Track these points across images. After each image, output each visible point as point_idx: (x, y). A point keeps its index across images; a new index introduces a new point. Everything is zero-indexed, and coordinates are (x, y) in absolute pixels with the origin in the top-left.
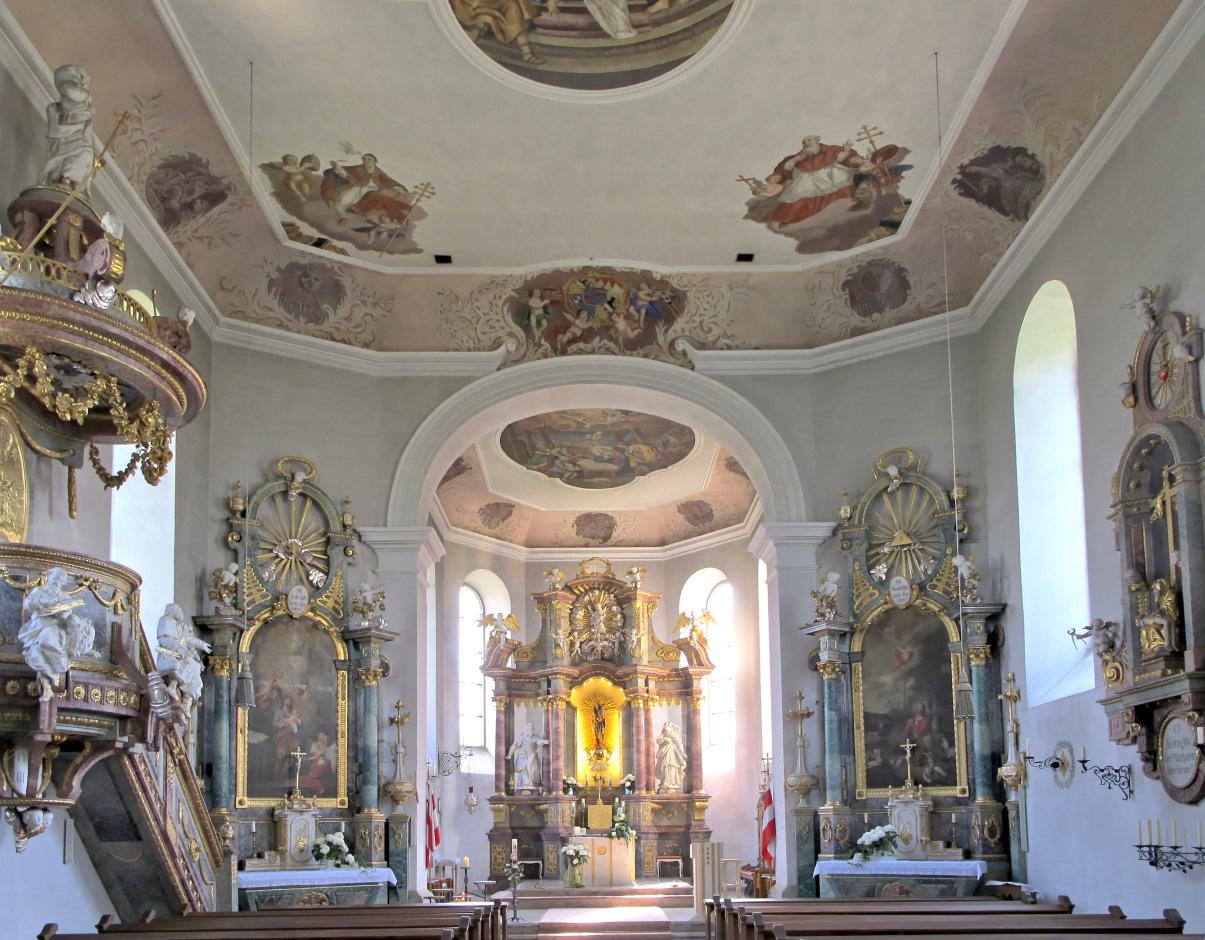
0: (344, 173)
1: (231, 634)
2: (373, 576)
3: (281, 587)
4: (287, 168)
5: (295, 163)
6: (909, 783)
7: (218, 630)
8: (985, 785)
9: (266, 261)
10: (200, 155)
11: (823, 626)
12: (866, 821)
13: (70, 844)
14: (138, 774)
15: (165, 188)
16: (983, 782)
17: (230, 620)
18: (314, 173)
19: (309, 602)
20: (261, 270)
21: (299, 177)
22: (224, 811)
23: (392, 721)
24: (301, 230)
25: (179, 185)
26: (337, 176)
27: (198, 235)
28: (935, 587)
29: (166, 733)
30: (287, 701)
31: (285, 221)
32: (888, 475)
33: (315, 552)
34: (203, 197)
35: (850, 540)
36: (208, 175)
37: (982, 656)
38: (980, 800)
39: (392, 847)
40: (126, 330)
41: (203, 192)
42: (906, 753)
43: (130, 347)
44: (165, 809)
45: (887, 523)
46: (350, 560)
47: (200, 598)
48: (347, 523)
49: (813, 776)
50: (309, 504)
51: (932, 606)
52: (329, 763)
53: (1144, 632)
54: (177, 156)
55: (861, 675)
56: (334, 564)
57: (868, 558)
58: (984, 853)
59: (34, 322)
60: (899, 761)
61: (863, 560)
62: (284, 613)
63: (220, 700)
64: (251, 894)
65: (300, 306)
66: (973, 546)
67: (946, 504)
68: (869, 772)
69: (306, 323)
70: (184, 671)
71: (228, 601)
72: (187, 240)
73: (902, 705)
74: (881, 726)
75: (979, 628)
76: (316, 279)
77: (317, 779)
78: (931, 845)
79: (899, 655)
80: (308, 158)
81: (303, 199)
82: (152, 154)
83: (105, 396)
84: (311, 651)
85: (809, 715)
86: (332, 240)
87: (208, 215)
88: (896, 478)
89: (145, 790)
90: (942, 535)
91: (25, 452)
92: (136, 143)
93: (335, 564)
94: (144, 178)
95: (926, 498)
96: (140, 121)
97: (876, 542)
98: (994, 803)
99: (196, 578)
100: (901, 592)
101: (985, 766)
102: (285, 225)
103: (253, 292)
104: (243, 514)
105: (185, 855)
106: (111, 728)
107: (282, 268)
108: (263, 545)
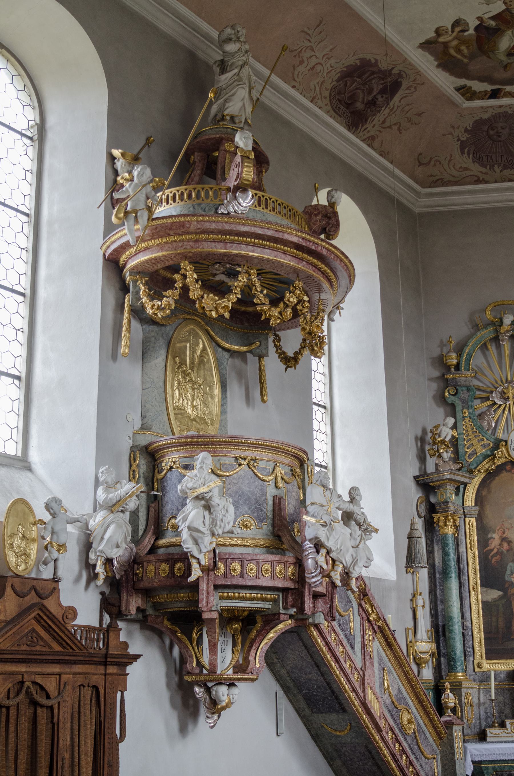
0: (492, 23)
1: (453, 489)
3: (500, 435)
4: (441, 39)
5: (447, 32)
7: (439, 487)
9: (453, 127)
10: (368, 57)
13: (282, 717)
14: (327, 644)
15: (347, 95)
17: (448, 476)
18: (466, 34)
20: (450, 137)
21: (455, 43)
22: (460, 676)
24: (474, 89)
25: (357, 89)
26: (487, 28)
27: (387, 124)
29: (360, 599)
31: (456, 85)
34: (383, 91)
36: (380, 71)
40: (255, 226)
41: (380, 87)
43: (263, 240)
44: (363, 680)
47: (422, 459)
54: (351, 65)
59: (183, 241)
62: (507, 460)
63: (446, 558)
64: (487, 768)
65: (494, 156)
69: (501, 171)
70: (331, 538)
71: (446, 456)
72: (378, 133)
76: (503, 128)
80: (457, 23)
81: (466, 61)
82: (329, 72)
83: (247, 290)
86: (504, 87)
87: (391, 105)
89: (337, 661)
91: (215, 353)
92: (313, 68)
94: (326, 93)
96: (313, 50)
99: (416, 438)
102: (458, 89)
103: (448, 159)
104: (457, 367)
105: (395, 726)
106: (275, 601)
107: (469, 128)
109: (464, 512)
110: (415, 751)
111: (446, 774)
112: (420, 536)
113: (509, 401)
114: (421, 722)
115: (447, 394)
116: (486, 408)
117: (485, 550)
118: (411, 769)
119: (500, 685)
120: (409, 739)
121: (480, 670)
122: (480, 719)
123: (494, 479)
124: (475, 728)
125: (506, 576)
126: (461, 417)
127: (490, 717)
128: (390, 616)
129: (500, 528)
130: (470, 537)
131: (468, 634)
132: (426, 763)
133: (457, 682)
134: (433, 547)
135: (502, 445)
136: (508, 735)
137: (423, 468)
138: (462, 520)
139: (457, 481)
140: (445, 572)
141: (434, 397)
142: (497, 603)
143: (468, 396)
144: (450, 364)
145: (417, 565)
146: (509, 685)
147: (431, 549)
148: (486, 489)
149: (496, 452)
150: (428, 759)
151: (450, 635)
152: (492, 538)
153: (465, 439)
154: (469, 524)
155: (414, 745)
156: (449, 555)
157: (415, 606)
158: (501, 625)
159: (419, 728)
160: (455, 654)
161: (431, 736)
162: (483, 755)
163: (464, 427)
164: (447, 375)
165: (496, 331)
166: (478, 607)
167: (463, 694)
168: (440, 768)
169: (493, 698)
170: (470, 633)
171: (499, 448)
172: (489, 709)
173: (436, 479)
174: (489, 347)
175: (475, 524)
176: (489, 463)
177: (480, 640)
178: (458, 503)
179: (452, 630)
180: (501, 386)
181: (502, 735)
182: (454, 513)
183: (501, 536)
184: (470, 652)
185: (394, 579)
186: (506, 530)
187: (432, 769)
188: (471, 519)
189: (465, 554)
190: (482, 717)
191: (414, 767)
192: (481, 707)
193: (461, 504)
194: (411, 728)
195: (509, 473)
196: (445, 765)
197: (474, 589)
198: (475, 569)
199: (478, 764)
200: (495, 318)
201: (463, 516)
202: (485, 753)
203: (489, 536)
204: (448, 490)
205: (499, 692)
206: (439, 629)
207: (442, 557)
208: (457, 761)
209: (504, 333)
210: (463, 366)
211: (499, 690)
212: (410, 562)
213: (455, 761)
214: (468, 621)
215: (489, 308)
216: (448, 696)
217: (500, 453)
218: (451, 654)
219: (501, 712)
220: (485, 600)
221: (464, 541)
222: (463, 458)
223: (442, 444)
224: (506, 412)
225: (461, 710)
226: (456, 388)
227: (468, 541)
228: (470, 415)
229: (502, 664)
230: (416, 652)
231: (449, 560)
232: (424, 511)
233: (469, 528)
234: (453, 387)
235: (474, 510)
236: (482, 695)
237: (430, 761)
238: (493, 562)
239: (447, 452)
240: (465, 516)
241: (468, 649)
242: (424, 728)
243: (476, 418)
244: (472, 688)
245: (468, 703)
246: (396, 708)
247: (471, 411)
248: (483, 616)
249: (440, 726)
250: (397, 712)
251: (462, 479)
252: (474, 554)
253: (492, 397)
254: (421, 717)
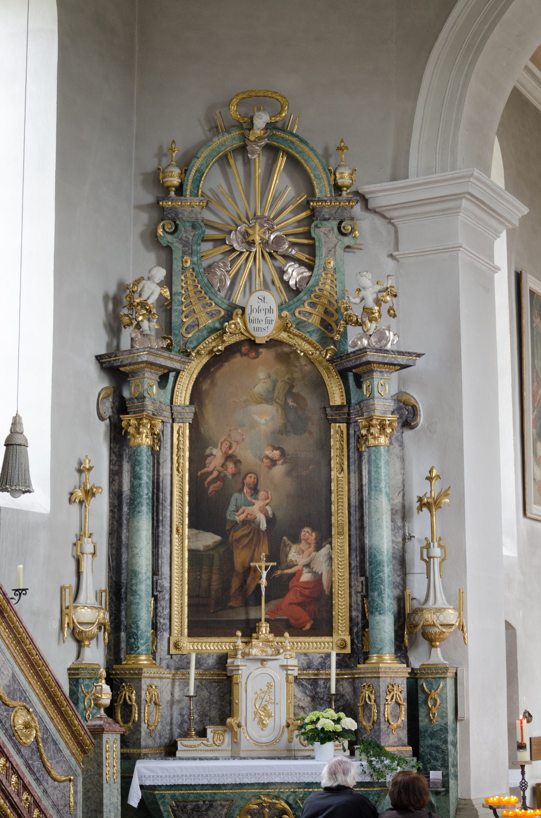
2: (391, 263)
3: (238, 299)
7: (134, 373)
19: (280, 317)
23: (423, 504)
30: (250, 479)
33: (295, 235)
39: (423, 722)
46: (347, 240)
48: (340, 182)
50: (282, 161)
52: (318, 578)
53: (328, 357)
56: (322, 252)
62: (243, 338)
63: (136, 482)
64: (163, 796)
77: (299, 604)
84: (289, 393)
93: (324, 251)
99: (106, 298)
104: (180, 190)
108: (210, 232)
109: (172, 414)
110: (35, 770)
111: (88, 803)
112: (23, 443)
113: (254, 247)
114: (51, 726)
115: (160, 231)
116: (221, 257)
117: (199, 473)
118: (25, 796)
119: (205, 675)
120: (26, 752)
121: (177, 652)
122: (171, 724)
123: (222, 366)
124: (160, 738)
125: (228, 513)
126: (180, 268)
127: (186, 722)
128: (21, 566)
129: (225, 440)
130: (178, 452)
131: (164, 598)
132: (55, 788)
133: (136, 669)
134: (121, 466)
135: (237, 315)
136: (208, 748)
137: (115, 343)
138: (169, 425)
139: (161, 366)
140: (134, 504)
141: (142, 235)
142: (211, 553)
143: (194, 236)
144: (169, 184)
145: (13, 488)
146: (219, 675)
147: (116, 468)
148: (209, 381)
149: (227, 324)
150: (59, 782)
151: (132, 598)
152: (212, 455)
153: (182, 303)
154: (178, 433)
155: (34, 761)
156: (140, 479)
157: (79, 553)
158: (215, 585)
159: (45, 736)
160: (138, 627)
161: (68, 748)
162: (158, 776)
163: (183, 285)
164: (162, 201)
165: (244, 137)
166: (182, 558)
167: (144, 687)
168: (80, 796)
169: (192, 693)
170: (167, 597)
171: (232, 319)
172: (186, 709)
173: (128, 362)
174: (232, 161)
175: (187, 432)
176: (217, 341)
177: (182, 607)
178: (162, 400)
179: (136, 592)
180: (244, 223)
181: (199, 748)
182: (154, 414)
183: (225, 453)
184: (164, 624)
185: (45, 512)
186: (234, 444)
187: (65, 796)
188: (181, 424)
189: (168, 478)
190: (174, 722)
191: (30, 793)
192: (175, 707)
193: (168, 402)
194: (30, 734)
195: (245, 358)
196: (88, 791)
197: (178, 531)
198: (182, 502)
199: (150, 789)
200: (243, 117)
201: (171, 420)
202: (160, 774)
203: (208, 452)
204: (146, 379)
205: (202, 685)
206: (120, 590)
207: (131, 481)
208: (105, 785)
209: (254, 141)
210: (188, 188)
211: (204, 682)
212: (4, 482)
213: (102, 785)
214: (166, 578)
215: (235, 101)
216: (101, 689)
217: (233, 326)
218: (131, 627)
219: (203, 715)
220: (193, 548)
221: (169, 458)
222: (177, 332)
223: (142, 307)
224: (250, 264)
225: (139, 710)
226: (175, 222)
227: (175, 458)
228: (194, 266)
229: (212, 644)
230: (73, 622)
231: (140, 485)
232: (110, 410)
233: (178, 439)
234: (171, 221)
235: (187, 411)
236: (177, 689)
237: (62, 784)
238: (210, 491)
239: (149, 320)
240: (173, 420)
241: (162, 621)
242: (57, 736)
243: (202, 270)
244: (161, 678)
245: (151, 700)
246: (6, 705)
247: (195, 259)
248: (189, 572)
249: (83, 733)
250: (6, 711)
251: (169, 364)
252: (182, 478)
253: (230, 240)
254: (52, 719)
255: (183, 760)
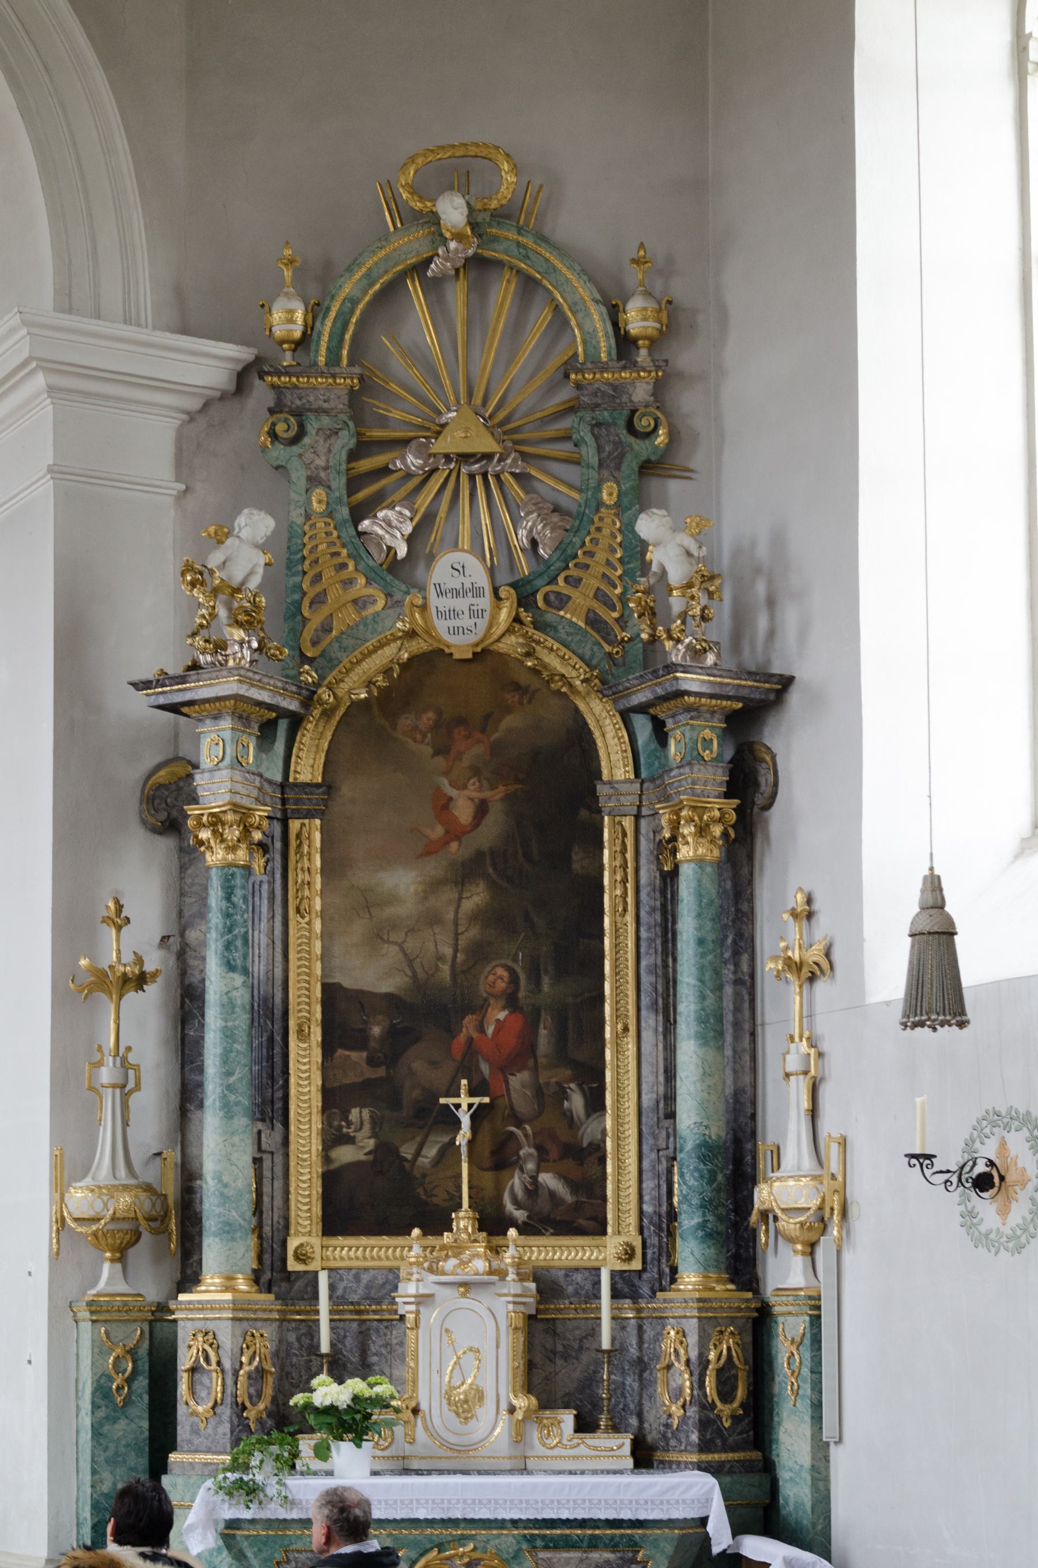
6: (463, 1220)
8: (709, 1236)
11: (227, 686)
12: (325, 1348)
16: (702, 1226)
28: (562, 601)
32: (434, 219)
35: (298, 414)
37: (717, 830)
38: (690, 1279)
42: (457, 1124)
45: (414, 376)
49: (148, 1188)
51: (553, 662)
55: (318, 862)
57: (354, 484)
58: (704, 1447)
60: (431, 1152)
61: (339, 483)
66: (674, 487)
67: (605, 346)
68: (331, 1179)
73: (446, 969)
74: (376, 1030)
75: (707, 743)
78: (539, 1421)
79: (444, 806)
85: (141, 980)
88: (459, 237)
90: (589, 439)
95: (540, 318)
97: (377, 434)
98: (723, 1289)
100: (461, 604)
101: (712, 1179)
255: (576, 1474)
